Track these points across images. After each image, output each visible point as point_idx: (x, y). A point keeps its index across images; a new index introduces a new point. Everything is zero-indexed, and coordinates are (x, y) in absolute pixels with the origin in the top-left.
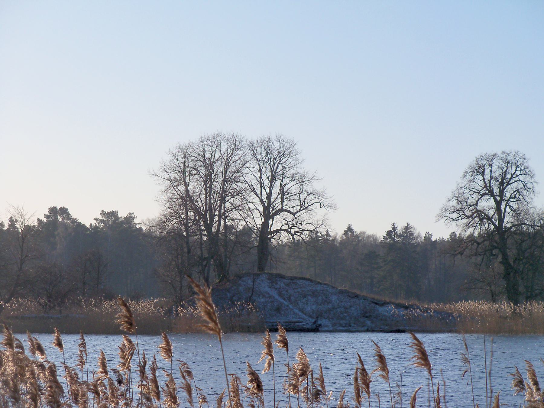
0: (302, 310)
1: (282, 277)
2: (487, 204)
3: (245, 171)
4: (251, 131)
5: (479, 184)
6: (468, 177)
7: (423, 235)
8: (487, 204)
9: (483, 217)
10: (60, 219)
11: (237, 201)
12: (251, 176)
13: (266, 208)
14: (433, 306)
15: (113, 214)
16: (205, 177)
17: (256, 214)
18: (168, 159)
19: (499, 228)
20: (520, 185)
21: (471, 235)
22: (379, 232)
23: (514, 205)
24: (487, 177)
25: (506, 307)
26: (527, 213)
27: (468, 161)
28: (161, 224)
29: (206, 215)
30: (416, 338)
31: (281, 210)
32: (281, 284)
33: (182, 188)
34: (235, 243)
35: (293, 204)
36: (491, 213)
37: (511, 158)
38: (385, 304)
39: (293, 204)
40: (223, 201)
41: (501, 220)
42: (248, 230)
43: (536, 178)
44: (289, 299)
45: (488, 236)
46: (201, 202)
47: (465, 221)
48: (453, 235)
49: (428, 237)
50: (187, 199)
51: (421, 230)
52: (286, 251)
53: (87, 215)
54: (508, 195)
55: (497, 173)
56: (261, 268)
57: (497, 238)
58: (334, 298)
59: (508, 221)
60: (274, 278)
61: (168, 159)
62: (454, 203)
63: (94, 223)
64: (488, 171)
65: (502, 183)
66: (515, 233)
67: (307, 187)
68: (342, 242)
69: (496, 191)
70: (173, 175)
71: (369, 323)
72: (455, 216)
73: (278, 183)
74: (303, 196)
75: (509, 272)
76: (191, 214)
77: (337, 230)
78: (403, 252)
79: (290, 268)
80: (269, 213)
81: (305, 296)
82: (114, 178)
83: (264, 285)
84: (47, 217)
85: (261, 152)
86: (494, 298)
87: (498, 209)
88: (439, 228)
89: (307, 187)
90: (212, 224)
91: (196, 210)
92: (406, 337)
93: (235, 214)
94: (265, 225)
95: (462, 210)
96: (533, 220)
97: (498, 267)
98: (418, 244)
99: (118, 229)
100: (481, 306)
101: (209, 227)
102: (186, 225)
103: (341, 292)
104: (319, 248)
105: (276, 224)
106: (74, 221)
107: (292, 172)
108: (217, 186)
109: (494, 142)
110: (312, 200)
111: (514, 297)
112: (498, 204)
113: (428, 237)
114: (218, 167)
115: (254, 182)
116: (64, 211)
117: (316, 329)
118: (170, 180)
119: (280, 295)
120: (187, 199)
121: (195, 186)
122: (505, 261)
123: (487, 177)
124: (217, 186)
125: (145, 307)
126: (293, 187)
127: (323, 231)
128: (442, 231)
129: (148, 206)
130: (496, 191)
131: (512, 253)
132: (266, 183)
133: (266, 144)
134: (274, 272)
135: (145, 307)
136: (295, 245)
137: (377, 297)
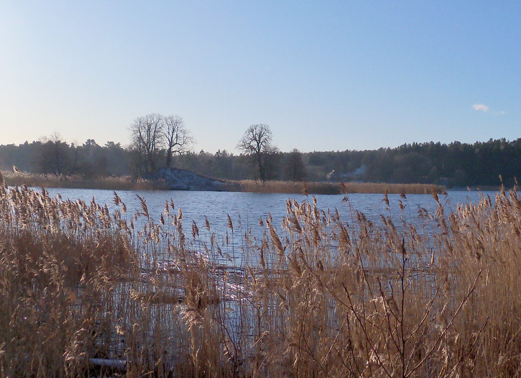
0: (183, 182)
1: (176, 169)
2: (254, 144)
3: (163, 128)
4: (166, 114)
5: (251, 136)
6: (247, 133)
7: (230, 154)
8: (254, 144)
9: (252, 148)
10: (91, 144)
11: (159, 139)
12: (165, 130)
13: (171, 143)
14: (233, 181)
15: (112, 143)
16: (148, 130)
17: (167, 145)
18: (133, 123)
19: (258, 153)
20: (267, 137)
21: (248, 155)
22: (213, 152)
23: (264, 144)
24: (254, 133)
25: (259, 182)
26: (269, 147)
27: (248, 127)
28: (130, 147)
29: (147, 145)
30: (116, 194)
31: (176, 144)
32: (175, 172)
33: (139, 134)
34: (159, 155)
35: (180, 142)
36: (255, 147)
37: (263, 126)
38: (215, 180)
39: (180, 142)
40: (154, 139)
41: (259, 150)
42: (163, 150)
43: (272, 134)
44: (178, 178)
45: (253, 155)
46: (145, 140)
47: (246, 149)
48: (241, 154)
49: (232, 155)
50: (140, 138)
51: (229, 152)
52: (178, 159)
53: (102, 143)
54: (262, 140)
55: (258, 132)
56: (168, 166)
57: (257, 156)
58: (195, 178)
59: (262, 150)
60: (173, 170)
61: (133, 123)
62: (242, 143)
63: (104, 146)
64: (254, 131)
65: (260, 136)
66: (264, 154)
67: (186, 135)
68: (199, 155)
69: (258, 139)
70: (135, 129)
71: (208, 187)
72: (242, 147)
73: (175, 133)
74: (185, 138)
75: (261, 170)
76: (141, 144)
77: (197, 151)
78: (222, 161)
79: (179, 165)
80: (171, 145)
81: (184, 176)
82: (115, 130)
83: (169, 172)
84: (86, 143)
85: (169, 121)
86: (256, 179)
87: (258, 145)
88: (235, 150)
89: (186, 135)
90: (149, 148)
91: (144, 142)
92: (111, 192)
93: (158, 145)
94: (170, 149)
95: (245, 145)
96: (271, 150)
97: (257, 167)
98: (227, 158)
99: (114, 149)
100: (250, 182)
101: (148, 149)
102: (140, 148)
103: (198, 175)
104: (190, 158)
105: (174, 149)
106: (97, 145)
107: (181, 129)
108: (152, 134)
109: (257, 121)
110: (188, 140)
111: (263, 178)
112: (258, 144)
113: (232, 155)
114: (153, 127)
115: (166, 133)
116: (93, 141)
117: (188, 189)
118: (134, 131)
119: (175, 176)
120: (140, 138)
121: (144, 133)
122: (260, 165)
123: (254, 133)
124: (152, 134)
125: (122, 179)
126: (181, 135)
127: (192, 152)
128: (237, 153)
129: (126, 141)
130: (258, 139)
131: (263, 162)
132: (171, 133)
133: (171, 118)
134: (173, 167)
135: (122, 179)
136: (181, 157)
137: (211, 177)
